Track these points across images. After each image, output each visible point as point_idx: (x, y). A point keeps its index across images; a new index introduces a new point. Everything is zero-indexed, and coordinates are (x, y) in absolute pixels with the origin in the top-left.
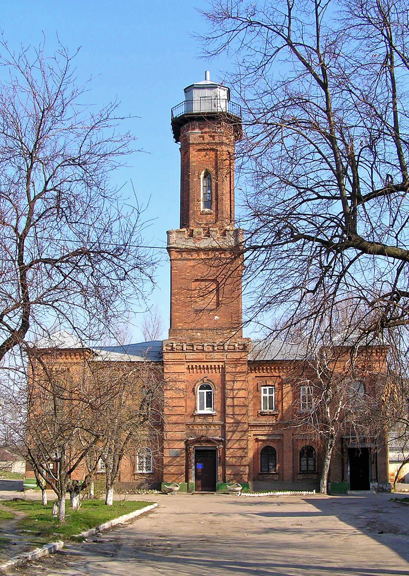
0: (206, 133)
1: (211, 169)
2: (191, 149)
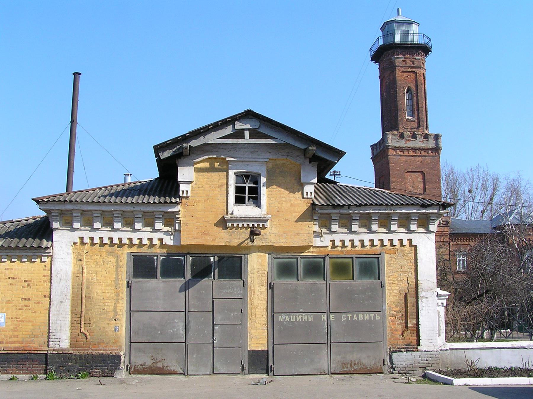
0: (407, 58)
1: (413, 87)
2: (397, 70)
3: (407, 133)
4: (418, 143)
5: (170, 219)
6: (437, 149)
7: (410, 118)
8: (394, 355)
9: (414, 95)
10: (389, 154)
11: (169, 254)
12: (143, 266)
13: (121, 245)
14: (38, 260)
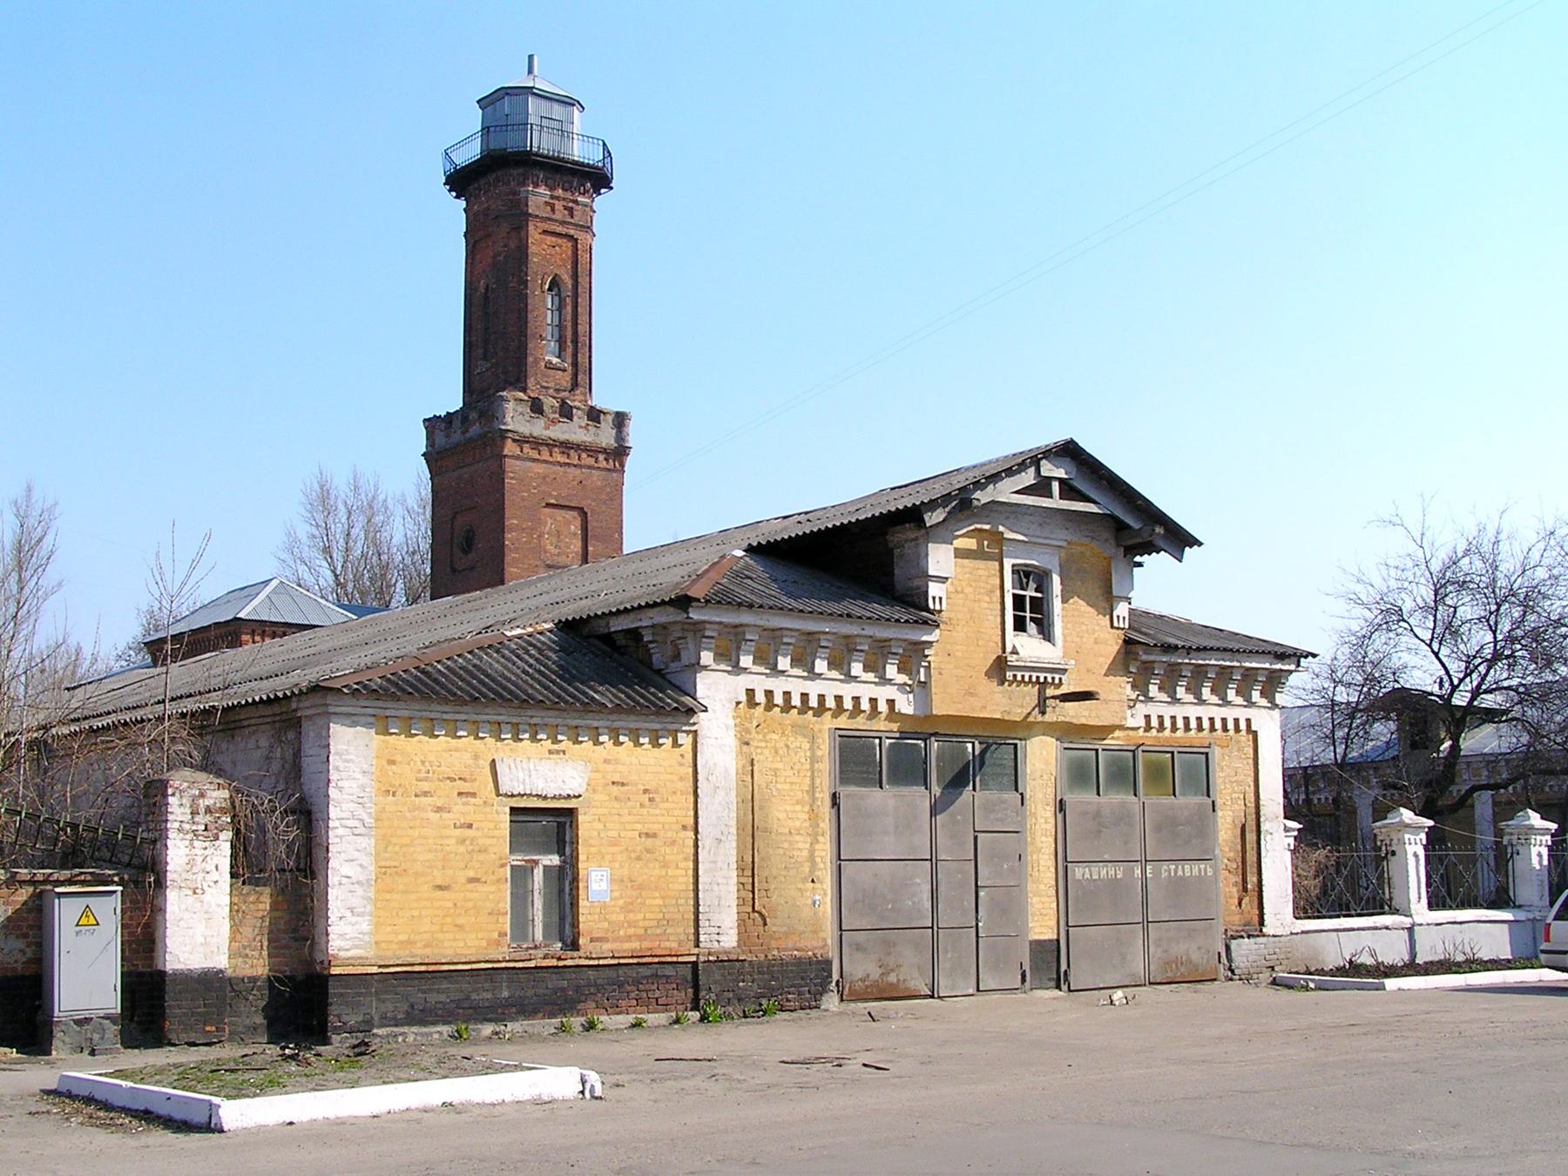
0: (558, 198)
3: (549, 403)
4: (574, 431)
5: (912, 657)
6: (620, 452)
7: (555, 360)
8: (1234, 944)
9: (568, 300)
10: (506, 452)
11: (904, 735)
12: (856, 760)
13: (821, 709)
14: (667, 742)
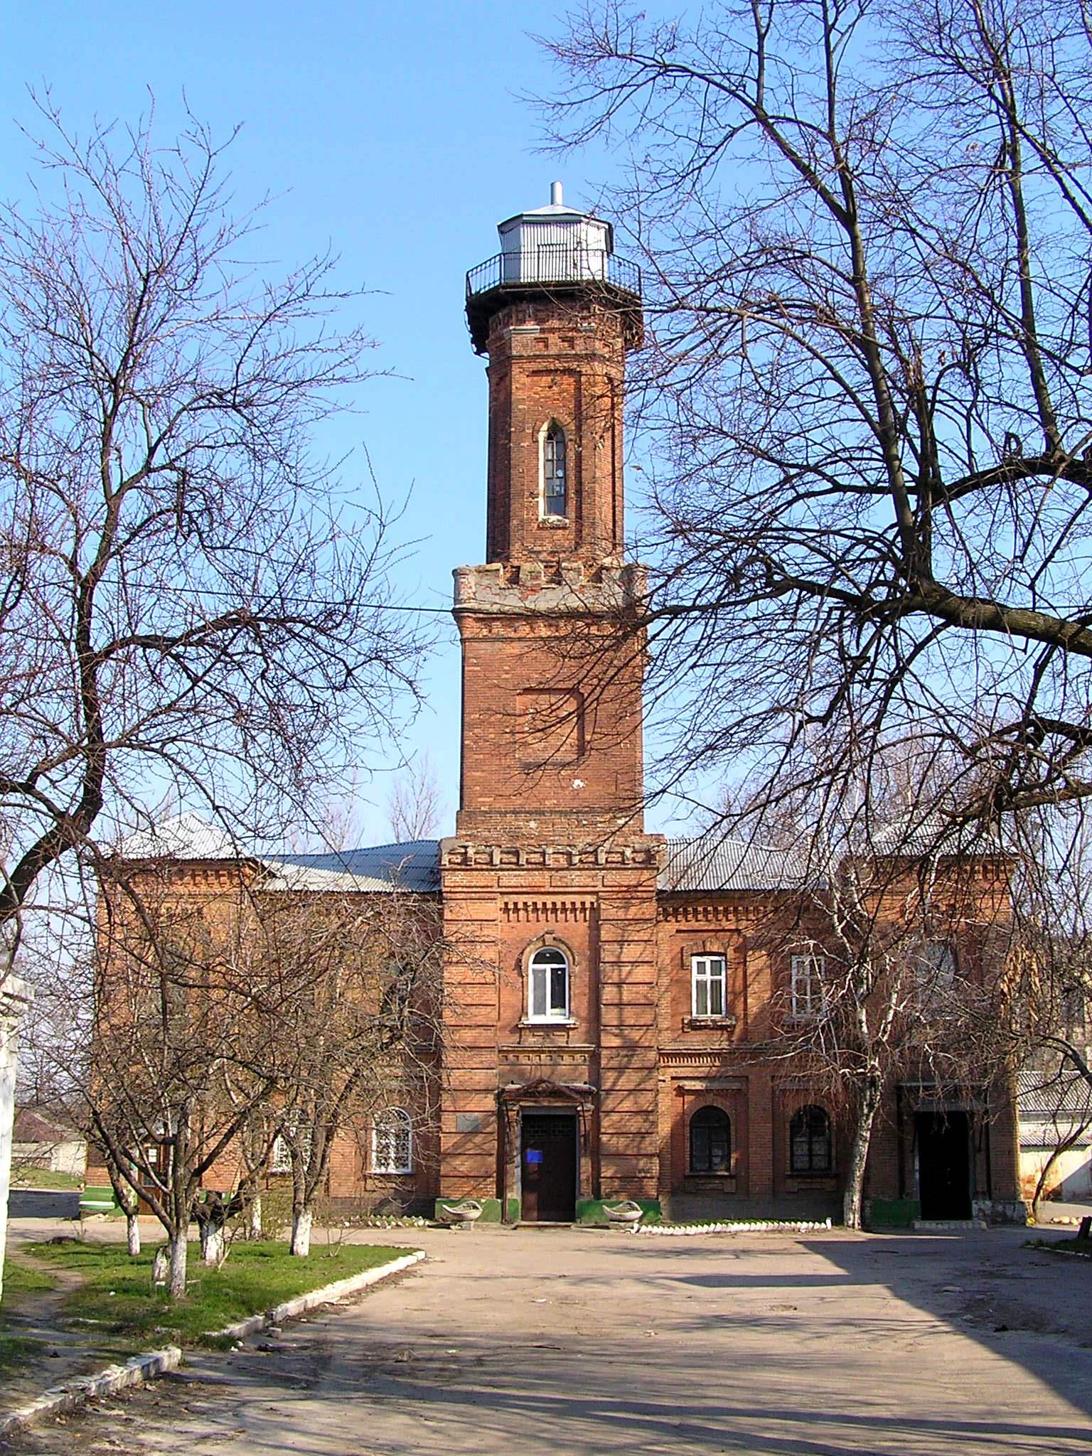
0: (552, 330)
1: (566, 419)
2: (515, 370)
7: (554, 518)
